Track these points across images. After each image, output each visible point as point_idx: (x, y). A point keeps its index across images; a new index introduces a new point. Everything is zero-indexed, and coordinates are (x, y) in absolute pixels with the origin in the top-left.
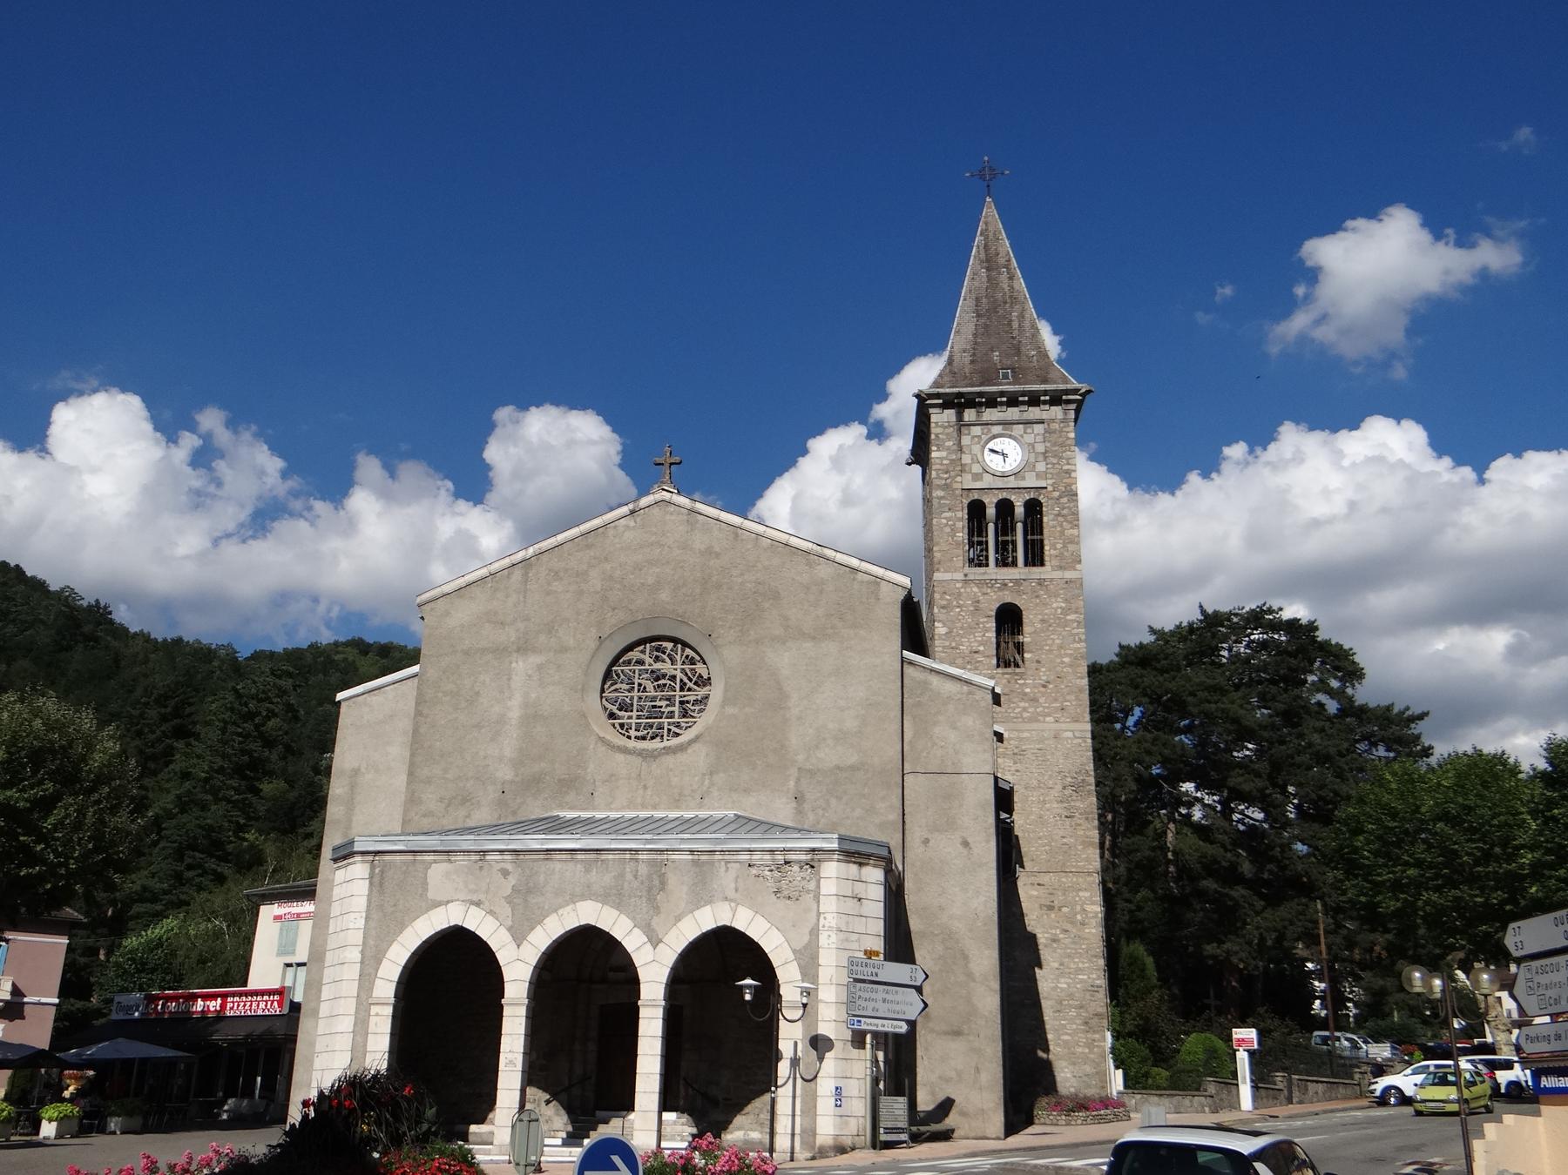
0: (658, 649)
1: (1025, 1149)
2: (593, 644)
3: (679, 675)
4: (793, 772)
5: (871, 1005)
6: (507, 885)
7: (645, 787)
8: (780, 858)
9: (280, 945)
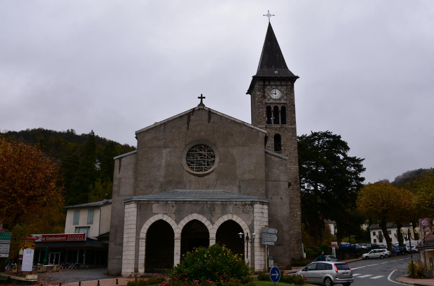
2: (184, 146)
5: (267, 238)
6: (174, 210)
9: (74, 222)
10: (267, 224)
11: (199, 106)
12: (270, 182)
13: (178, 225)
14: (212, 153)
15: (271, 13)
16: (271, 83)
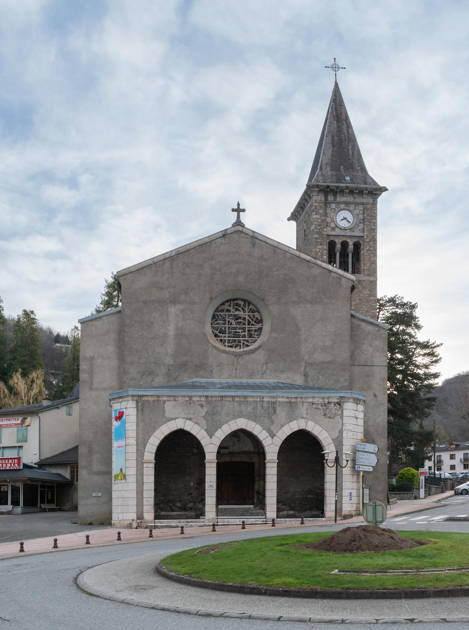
0: (237, 304)
1: (405, 514)
3: (247, 318)
4: (303, 363)
6: (203, 412)
7: (236, 369)
8: (326, 401)
10: (361, 436)
11: (234, 225)
12: (357, 367)
13: (211, 438)
14: (257, 315)
15: (341, 63)
16: (338, 199)
